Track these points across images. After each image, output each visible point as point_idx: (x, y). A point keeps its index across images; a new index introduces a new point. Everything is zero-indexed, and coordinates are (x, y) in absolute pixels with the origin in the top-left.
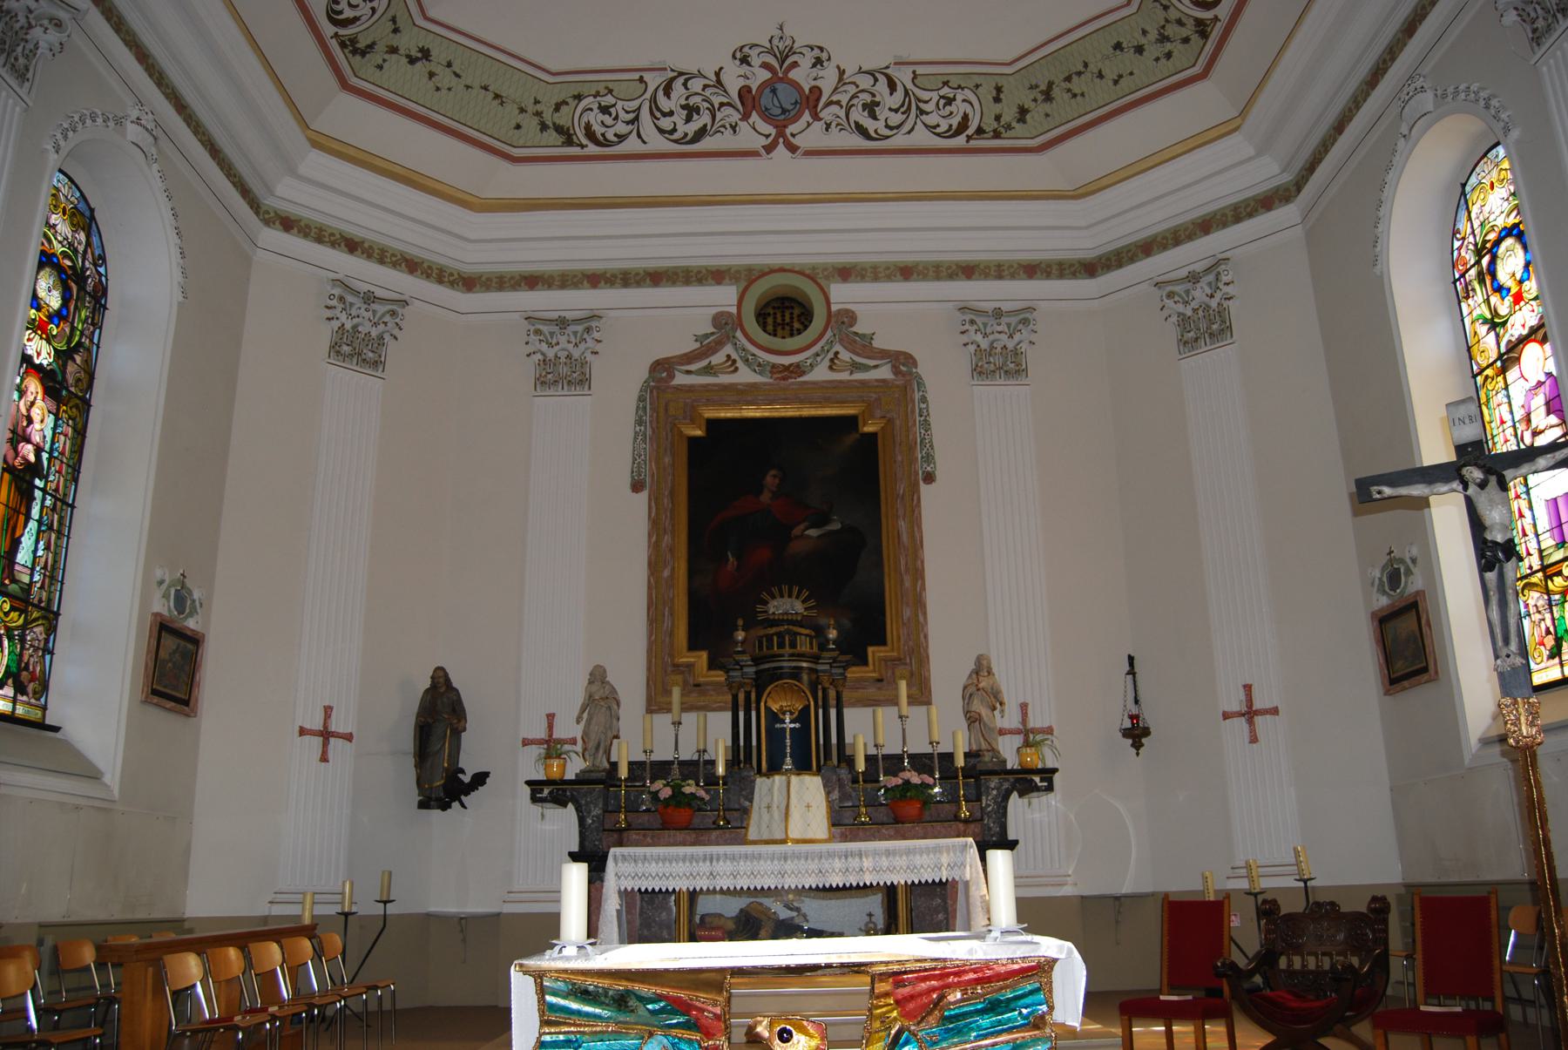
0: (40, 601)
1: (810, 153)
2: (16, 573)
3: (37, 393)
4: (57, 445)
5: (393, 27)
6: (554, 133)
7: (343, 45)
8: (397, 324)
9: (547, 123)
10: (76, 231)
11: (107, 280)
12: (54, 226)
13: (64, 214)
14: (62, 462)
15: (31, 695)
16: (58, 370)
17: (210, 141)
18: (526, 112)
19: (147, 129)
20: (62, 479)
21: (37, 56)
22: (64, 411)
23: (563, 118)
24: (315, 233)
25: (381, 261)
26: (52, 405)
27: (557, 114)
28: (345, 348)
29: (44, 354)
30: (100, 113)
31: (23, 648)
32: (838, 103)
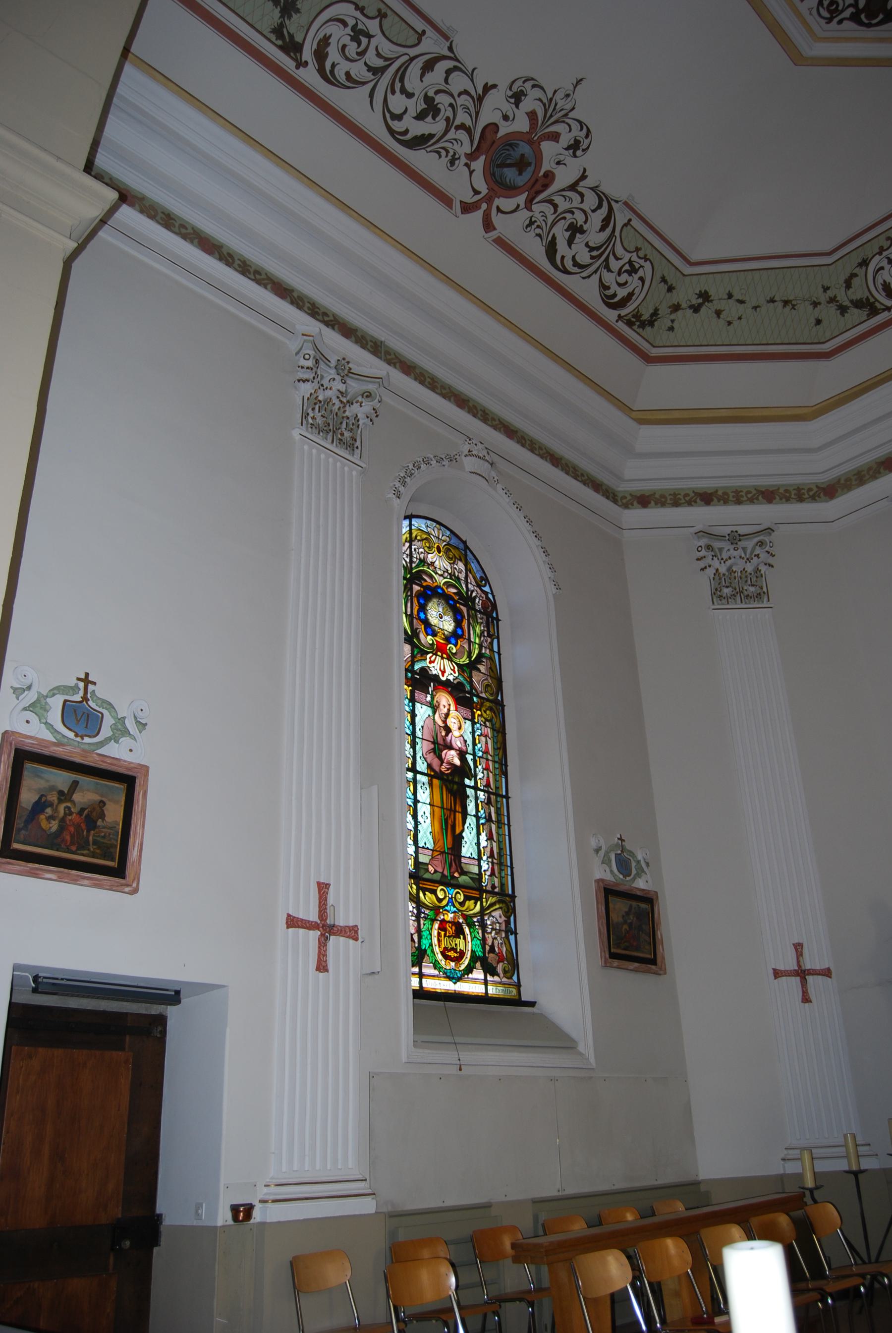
0: (493, 887)
1: (500, 242)
2: (462, 865)
3: (450, 705)
4: (479, 746)
5: (666, 287)
6: (856, 311)
7: (630, 324)
8: (768, 552)
9: (844, 304)
10: (454, 563)
11: (494, 596)
12: (432, 564)
13: (439, 551)
14: (487, 760)
15: (502, 975)
16: (465, 682)
17: (547, 452)
18: (820, 303)
19: (479, 457)
20: (491, 775)
21: (360, 427)
22: (478, 715)
23: (858, 292)
24: (671, 499)
25: (739, 502)
26: (467, 713)
27: (851, 290)
28: (726, 591)
29: (448, 671)
30: (432, 456)
31: (484, 931)
32: (555, 206)
